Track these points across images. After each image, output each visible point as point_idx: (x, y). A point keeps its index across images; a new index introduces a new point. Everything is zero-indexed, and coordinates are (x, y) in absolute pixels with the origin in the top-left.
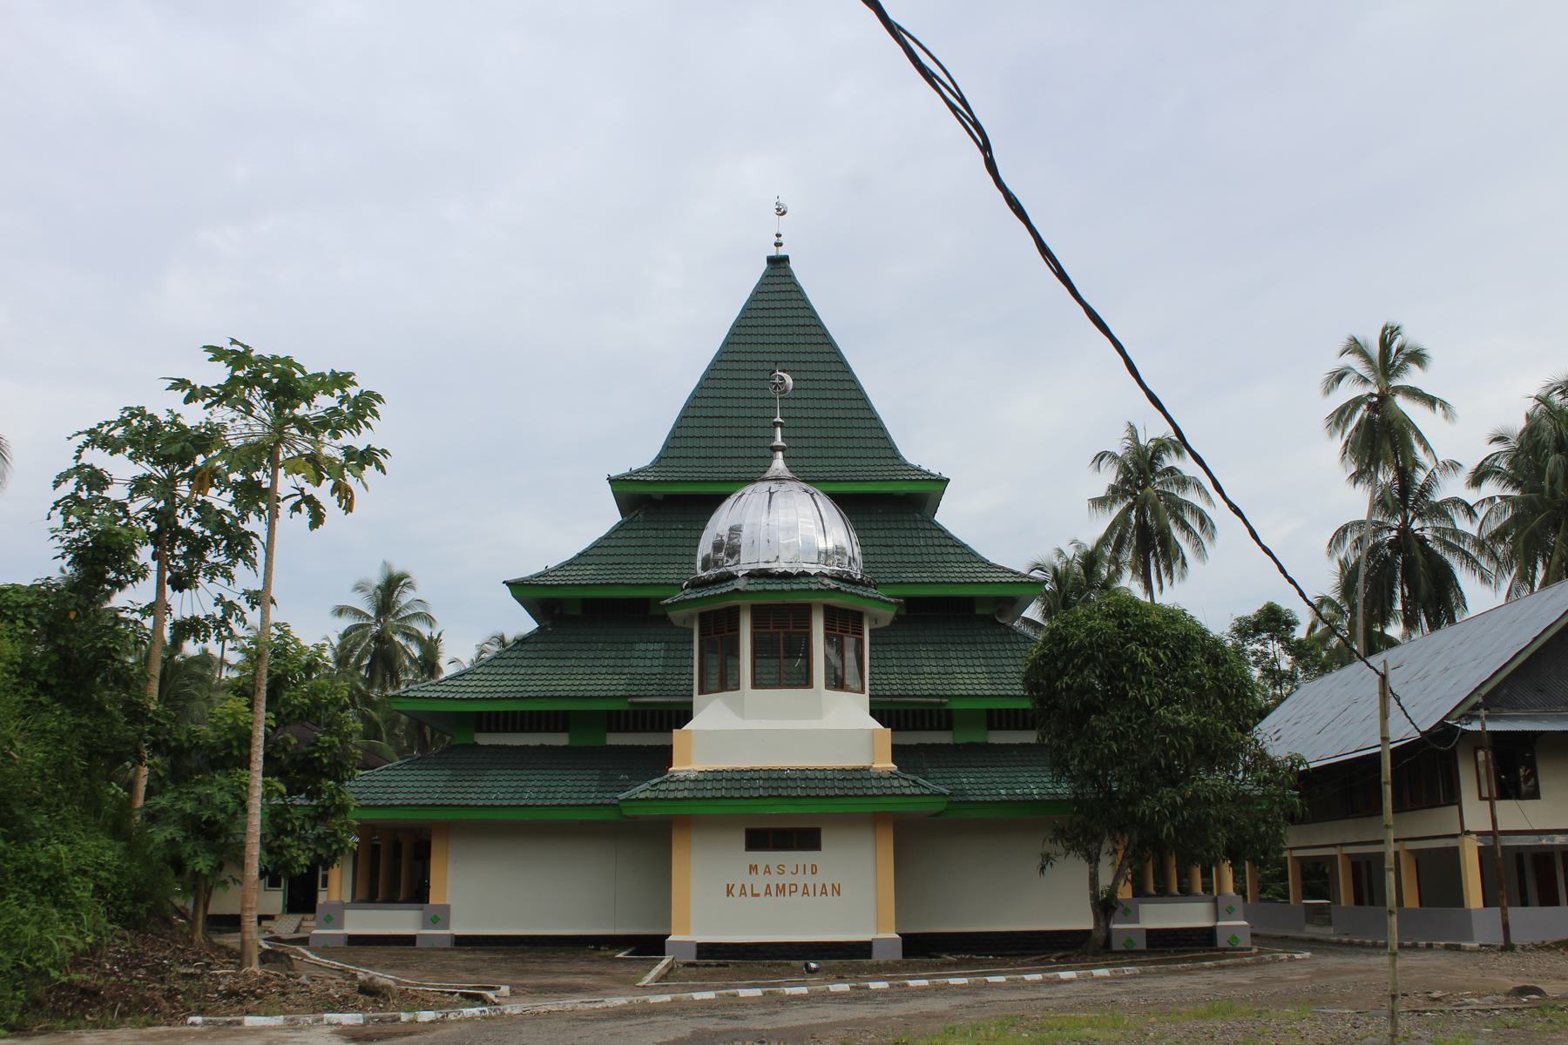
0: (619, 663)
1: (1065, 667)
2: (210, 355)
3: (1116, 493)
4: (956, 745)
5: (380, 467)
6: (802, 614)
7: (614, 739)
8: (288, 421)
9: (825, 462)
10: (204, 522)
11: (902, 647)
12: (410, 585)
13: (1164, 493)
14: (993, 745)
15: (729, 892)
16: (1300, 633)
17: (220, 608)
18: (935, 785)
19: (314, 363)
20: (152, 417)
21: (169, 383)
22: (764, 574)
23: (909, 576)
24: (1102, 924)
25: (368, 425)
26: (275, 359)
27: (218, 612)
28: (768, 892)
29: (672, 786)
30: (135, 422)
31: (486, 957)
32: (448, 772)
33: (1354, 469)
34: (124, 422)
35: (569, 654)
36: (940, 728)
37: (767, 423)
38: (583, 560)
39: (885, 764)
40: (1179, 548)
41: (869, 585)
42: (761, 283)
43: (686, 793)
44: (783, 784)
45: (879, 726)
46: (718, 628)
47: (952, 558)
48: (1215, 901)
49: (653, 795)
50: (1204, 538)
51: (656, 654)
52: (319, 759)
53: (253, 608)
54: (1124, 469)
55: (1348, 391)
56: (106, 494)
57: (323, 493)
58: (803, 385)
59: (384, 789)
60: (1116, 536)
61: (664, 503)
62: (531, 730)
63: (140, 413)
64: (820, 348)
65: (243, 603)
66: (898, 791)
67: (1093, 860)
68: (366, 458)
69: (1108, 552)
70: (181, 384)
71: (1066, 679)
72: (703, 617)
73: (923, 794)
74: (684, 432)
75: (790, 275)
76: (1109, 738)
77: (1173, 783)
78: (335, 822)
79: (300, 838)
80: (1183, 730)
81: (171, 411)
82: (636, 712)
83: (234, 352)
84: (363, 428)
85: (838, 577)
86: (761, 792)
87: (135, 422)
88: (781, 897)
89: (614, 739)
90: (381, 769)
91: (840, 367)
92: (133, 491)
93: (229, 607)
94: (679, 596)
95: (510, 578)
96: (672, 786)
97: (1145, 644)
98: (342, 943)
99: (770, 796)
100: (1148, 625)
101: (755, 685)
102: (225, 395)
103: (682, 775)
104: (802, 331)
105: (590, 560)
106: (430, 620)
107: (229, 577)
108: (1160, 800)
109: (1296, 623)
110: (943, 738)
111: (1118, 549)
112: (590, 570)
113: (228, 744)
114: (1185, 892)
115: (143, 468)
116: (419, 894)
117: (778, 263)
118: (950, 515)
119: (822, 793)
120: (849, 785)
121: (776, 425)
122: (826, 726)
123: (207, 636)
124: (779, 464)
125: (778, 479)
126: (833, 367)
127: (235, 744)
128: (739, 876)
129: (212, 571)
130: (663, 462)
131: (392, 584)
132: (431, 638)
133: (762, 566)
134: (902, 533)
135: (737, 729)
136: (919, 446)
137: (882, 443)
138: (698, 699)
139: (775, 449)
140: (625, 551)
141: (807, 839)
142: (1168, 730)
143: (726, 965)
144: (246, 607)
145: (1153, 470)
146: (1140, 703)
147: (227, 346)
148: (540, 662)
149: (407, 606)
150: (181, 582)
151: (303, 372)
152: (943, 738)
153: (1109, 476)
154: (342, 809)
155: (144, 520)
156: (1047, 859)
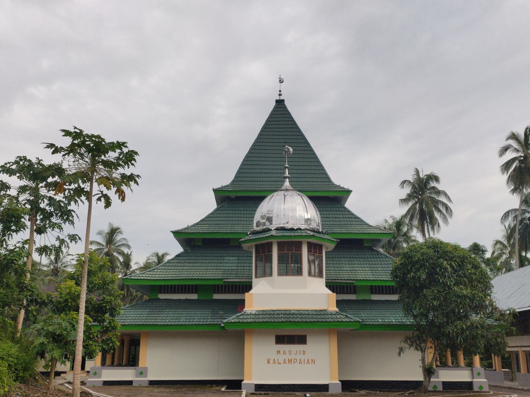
0: (219, 265)
1: (411, 269)
2: (63, 133)
3: (410, 197)
4: (357, 300)
5: (136, 182)
6: (299, 245)
7: (216, 296)
8: (99, 162)
9: (301, 183)
10: (50, 205)
11: (334, 259)
12: (121, 233)
13: (430, 197)
14: (373, 301)
15: (268, 362)
16: (488, 255)
17: (58, 242)
18: (353, 316)
19: (109, 139)
20: (30, 161)
21: (45, 145)
22: (283, 229)
23: (337, 230)
24: (428, 379)
25: (133, 164)
26: (93, 136)
27: (57, 244)
28: (285, 362)
29: (245, 317)
30: (21, 163)
31: (167, 390)
32: (147, 310)
33: (513, 187)
34: (16, 162)
35: (198, 261)
36: (350, 293)
37: (282, 167)
38: (203, 223)
39: (334, 308)
40: (437, 219)
41: (322, 233)
42: (274, 111)
43: (251, 320)
44: (291, 316)
45: (330, 292)
46: (263, 251)
47: (354, 223)
48: (472, 370)
49: (237, 321)
50: (447, 216)
51: (234, 261)
52: (105, 306)
53: (71, 242)
54: (414, 187)
55: (510, 155)
56: (8, 192)
57: (112, 193)
58: (297, 152)
59: (128, 317)
60: (411, 214)
61: (238, 198)
62: (182, 293)
63: (25, 158)
64: (298, 137)
65: (67, 239)
66: (340, 320)
67: (423, 351)
68: (132, 178)
69: (407, 221)
70: (51, 146)
71: (412, 274)
72: (256, 246)
73: (350, 321)
74: (243, 171)
75: (285, 107)
76: (432, 299)
77: (460, 319)
78: (110, 334)
79: (95, 341)
80: (465, 297)
81: (38, 158)
82: (225, 285)
83: (75, 132)
84: (131, 166)
85: (313, 231)
86: (283, 320)
87: (21, 163)
88: (290, 364)
89: (216, 296)
90: (116, 307)
91: (306, 145)
92: (19, 192)
93: (62, 242)
94: (247, 238)
95: (173, 230)
96: (245, 317)
97: (446, 260)
98: (101, 385)
99: (287, 321)
100: (447, 251)
101: (279, 274)
102: (71, 150)
103: (249, 312)
104: (290, 130)
105: (206, 223)
106: (129, 247)
107: (60, 228)
108: (456, 326)
109: (486, 251)
110: (353, 297)
111: (411, 219)
112: (206, 227)
113: (66, 301)
114: (456, 365)
115: (24, 182)
116: (133, 361)
117: (280, 103)
118: (351, 204)
119: (308, 320)
120: (319, 317)
121: (286, 167)
122: (307, 292)
123: (51, 253)
124: (287, 183)
125: (287, 190)
126: (303, 145)
127: (70, 300)
128: (273, 355)
129: (53, 226)
130: (235, 183)
131: (113, 232)
132: (128, 254)
133: (282, 225)
134: (333, 213)
135: (271, 293)
136: (338, 177)
137: (324, 176)
138: (254, 281)
139: (285, 178)
140: (220, 219)
141: (301, 340)
142: (459, 297)
143: (268, 394)
144: (69, 241)
145: (426, 188)
146: (445, 284)
147: (72, 130)
148: (186, 265)
149: (119, 241)
150: (40, 231)
151: (105, 142)
152: (353, 297)
153: (407, 190)
154: (114, 328)
155: (24, 205)
156: (401, 350)
